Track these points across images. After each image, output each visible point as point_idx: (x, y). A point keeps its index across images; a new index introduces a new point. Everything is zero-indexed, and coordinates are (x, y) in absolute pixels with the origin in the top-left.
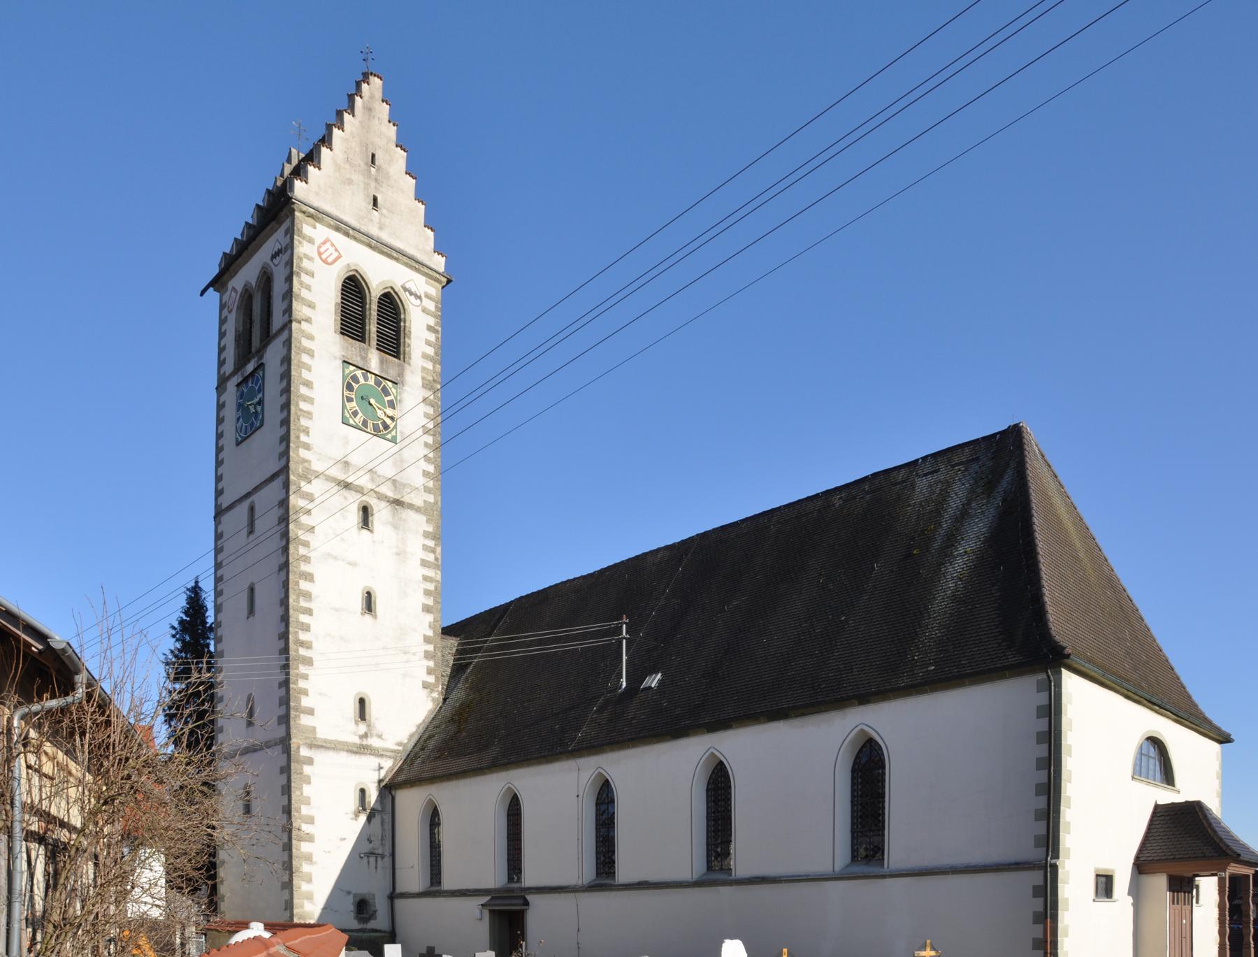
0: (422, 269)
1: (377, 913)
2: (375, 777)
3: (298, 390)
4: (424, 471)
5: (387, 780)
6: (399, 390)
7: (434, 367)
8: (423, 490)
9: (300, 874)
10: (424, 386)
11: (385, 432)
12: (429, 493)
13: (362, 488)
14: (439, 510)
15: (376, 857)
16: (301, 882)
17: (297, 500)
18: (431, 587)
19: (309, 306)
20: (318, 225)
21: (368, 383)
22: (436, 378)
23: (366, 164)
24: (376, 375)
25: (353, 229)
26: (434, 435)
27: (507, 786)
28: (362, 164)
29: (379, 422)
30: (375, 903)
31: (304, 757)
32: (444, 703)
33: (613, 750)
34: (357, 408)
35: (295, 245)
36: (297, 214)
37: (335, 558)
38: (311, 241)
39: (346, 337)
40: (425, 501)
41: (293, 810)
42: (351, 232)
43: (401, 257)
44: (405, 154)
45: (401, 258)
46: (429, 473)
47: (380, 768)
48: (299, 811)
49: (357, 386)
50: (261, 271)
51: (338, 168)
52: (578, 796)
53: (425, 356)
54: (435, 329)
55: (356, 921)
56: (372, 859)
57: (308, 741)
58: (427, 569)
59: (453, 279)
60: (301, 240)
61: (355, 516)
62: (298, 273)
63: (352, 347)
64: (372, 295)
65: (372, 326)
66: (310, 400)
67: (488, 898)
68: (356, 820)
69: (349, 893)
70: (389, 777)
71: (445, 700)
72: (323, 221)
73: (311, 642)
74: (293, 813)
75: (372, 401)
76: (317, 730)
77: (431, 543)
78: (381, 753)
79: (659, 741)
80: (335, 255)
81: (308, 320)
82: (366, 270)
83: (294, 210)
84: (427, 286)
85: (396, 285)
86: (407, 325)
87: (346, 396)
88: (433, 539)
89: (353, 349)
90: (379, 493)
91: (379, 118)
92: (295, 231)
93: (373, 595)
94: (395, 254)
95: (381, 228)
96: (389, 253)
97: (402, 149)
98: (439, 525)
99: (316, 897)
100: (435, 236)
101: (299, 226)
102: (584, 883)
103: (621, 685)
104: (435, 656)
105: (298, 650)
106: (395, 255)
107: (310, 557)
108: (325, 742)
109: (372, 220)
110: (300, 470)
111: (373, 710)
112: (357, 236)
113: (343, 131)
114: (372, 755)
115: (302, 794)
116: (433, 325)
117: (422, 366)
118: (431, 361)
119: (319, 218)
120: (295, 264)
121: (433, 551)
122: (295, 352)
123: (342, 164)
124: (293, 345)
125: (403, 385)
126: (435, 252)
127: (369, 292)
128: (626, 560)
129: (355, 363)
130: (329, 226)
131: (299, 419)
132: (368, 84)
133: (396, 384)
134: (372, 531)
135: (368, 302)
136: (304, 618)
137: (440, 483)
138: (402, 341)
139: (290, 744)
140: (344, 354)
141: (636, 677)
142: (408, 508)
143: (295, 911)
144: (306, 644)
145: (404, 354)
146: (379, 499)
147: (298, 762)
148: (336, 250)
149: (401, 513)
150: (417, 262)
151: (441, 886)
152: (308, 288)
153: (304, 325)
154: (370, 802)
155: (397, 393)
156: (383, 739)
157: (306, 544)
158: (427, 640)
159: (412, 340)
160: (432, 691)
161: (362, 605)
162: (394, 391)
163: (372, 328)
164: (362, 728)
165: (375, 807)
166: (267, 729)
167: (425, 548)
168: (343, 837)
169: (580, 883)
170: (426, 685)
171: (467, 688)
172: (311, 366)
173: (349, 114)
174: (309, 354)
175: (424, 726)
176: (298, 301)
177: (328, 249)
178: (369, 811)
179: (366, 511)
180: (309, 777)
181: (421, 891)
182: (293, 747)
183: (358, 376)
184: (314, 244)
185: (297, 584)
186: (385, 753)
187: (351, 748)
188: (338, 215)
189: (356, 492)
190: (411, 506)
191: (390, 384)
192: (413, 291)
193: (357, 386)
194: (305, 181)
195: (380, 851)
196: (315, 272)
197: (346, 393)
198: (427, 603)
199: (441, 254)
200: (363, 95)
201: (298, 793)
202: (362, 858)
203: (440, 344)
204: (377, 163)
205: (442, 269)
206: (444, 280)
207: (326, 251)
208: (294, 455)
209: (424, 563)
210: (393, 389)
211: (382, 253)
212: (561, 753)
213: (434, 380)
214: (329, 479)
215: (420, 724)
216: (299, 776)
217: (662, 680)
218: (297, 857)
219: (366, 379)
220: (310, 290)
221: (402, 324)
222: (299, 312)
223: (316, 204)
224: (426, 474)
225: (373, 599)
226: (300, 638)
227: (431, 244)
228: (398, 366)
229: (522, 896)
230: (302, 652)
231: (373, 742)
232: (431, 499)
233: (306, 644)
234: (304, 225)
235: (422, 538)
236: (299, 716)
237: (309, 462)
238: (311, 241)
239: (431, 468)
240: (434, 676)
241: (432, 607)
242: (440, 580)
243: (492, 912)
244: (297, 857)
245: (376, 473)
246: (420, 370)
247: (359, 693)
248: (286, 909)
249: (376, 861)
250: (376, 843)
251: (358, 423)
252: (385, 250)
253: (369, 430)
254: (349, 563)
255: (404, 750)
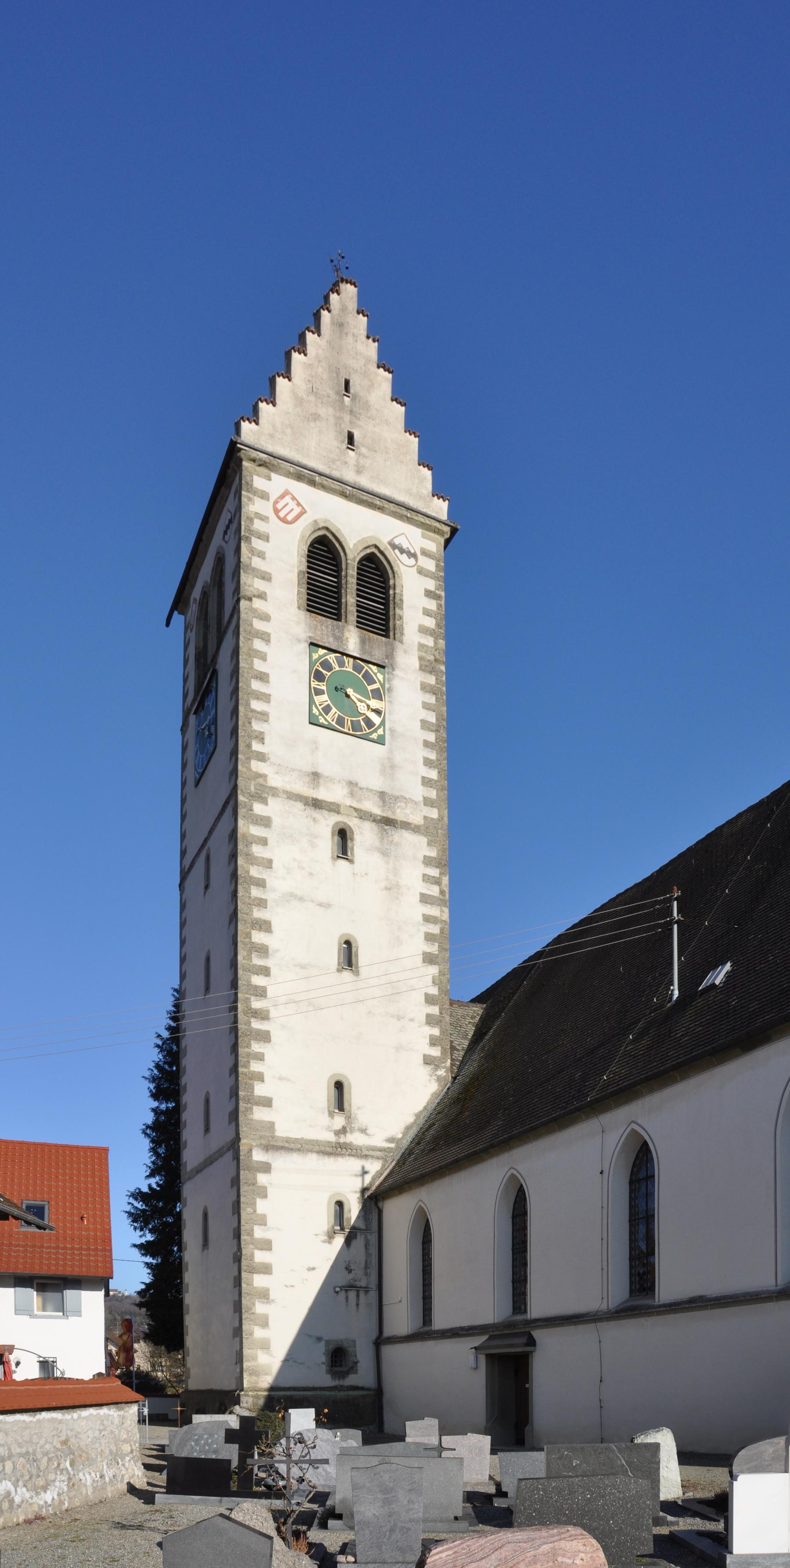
0: (416, 518)
1: (359, 1365)
2: (357, 1184)
3: (249, 686)
4: (423, 778)
5: (374, 1188)
6: (386, 675)
7: (435, 643)
8: (422, 803)
9: (252, 1317)
10: (422, 668)
11: (368, 731)
12: (432, 807)
13: (338, 806)
14: (445, 827)
15: (358, 1291)
16: (253, 1326)
17: (249, 827)
18: (435, 929)
19: (263, 578)
20: (274, 476)
21: (344, 669)
22: (438, 657)
23: (338, 393)
24: (355, 658)
25: (320, 474)
26: (437, 731)
27: (509, 1174)
28: (331, 393)
29: (360, 718)
30: (355, 1351)
31: (257, 1162)
32: (453, 1083)
33: (652, 1091)
34: (329, 702)
35: (243, 503)
36: (245, 464)
37: (301, 899)
38: (264, 496)
39: (313, 615)
40: (425, 818)
41: (242, 1232)
42: (318, 479)
43: (386, 505)
44: (390, 376)
45: (386, 506)
46: (430, 780)
47: (364, 1172)
48: (251, 1233)
49: (329, 674)
50: (216, 557)
51: (299, 401)
52: (602, 1173)
53: (423, 630)
54: (436, 595)
55: (329, 1376)
56: (352, 1295)
57: (263, 1142)
58: (429, 906)
59: (459, 527)
60: (250, 495)
61: (327, 843)
62: (247, 537)
63: (322, 625)
64: (348, 558)
65: (348, 597)
66: (265, 698)
67: (484, 1338)
68: (330, 1243)
69: (319, 1339)
70: (377, 1183)
71: (454, 1078)
72: (280, 468)
73: (268, 1011)
74: (242, 1237)
75: (350, 691)
76: (277, 1127)
77: (434, 872)
78: (365, 1152)
79: (721, 1061)
80: (297, 510)
81: (262, 596)
82: (339, 526)
83: (241, 460)
84: (425, 540)
85: (380, 541)
86: (397, 591)
87: (314, 687)
88: (437, 867)
89: (323, 627)
90: (361, 810)
91: (353, 335)
92: (243, 486)
93: (353, 945)
94: (378, 502)
95: (359, 471)
96: (370, 500)
97: (385, 370)
98: (445, 847)
99: (274, 1346)
100: (433, 475)
101: (248, 479)
102: (610, 1306)
103: (672, 995)
104: (441, 1021)
105: (250, 1022)
106: (378, 503)
107: (266, 901)
108: (287, 1142)
109: (346, 463)
110: (252, 788)
111: (355, 1097)
112: (325, 483)
113: (305, 355)
114: (353, 1156)
115: (255, 1211)
116: (433, 589)
117: (419, 643)
118: (431, 635)
119: (273, 465)
120: (243, 528)
121: (437, 882)
122: (244, 637)
123: (305, 397)
124: (241, 629)
125: (393, 669)
126: (433, 496)
127: (345, 554)
128: (694, 845)
129: (327, 645)
130: (288, 475)
131: (250, 723)
132: (339, 294)
133: (383, 667)
134: (351, 861)
135: (344, 567)
136: (258, 980)
137: (446, 792)
138: (391, 613)
139: (239, 1147)
140: (311, 634)
141: (690, 980)
142: (402, 828)
143: (246, 1365)
144: (261, 1013)
145: (394, 629)
146: (361, 818)
147: (249, 1168)
148: (299, 504)
149: (392, 835)
150: (409, 509)
151: (431, 1325)
152: (262, 555)
153: (257, 603)
154: (350, 1219)
155: (384, 678)
156: (367, 1134)
157: (261, 884)
158: (430, 1000)
159: (404, 611)
160: (437, 1067)
161: (339, 959)
162: (380, 677)
163: (350, 599)
164: (339, 1121)
165: (357, 1225)
166: (220, 1135)
167: (426, 878)
168: (311, 1266)
169: (604, 1307)
170: (428, 1060)
171: (482, 1058)
172: (266, 654)
173: (313, 333)
174: (262, 639)
175: (426, 1114)
176: (248, 574)
177: (287, 504)
178: (347, 1230)
179: (343, 835)
180: (264, 1188)
181: (410, 1332)
182: (243, 1149)
183: (331, 661)
184: (268, 500)
185: (249, 935)
186: (371, 1153)
187: (323, 1148)
188: (300, 460)
189: (330, 811)
190: (406, 826)
191: (374, 668)
192: (405, 547)
193: (329, 674)
194: (255, 421)
195: (363, 1283)
196: (270, 534)
197: (315, 684)
198: (428, 950)
199: (442, 497)
200: (332, 307)
201: (249, 1210)
202: (337, 1292)
203: (444, 613)
204: (352, 390)
205: (444, 516)
206: (447, 529)
207: (284, 506)
208: (245, 770)
209: (425, 899)
210: (378, 675)
211: (361, 502)
212: (578, 1109)
213: (436, 660)
214: (293, 796)
215: (421, 1112)
216: (251, 1187)
217: (731, 971)
218: (248, 1294)
219: (341, 664)
220: (264, 558)
221: (391, 592)
222: (249, 586)
223: (270, 448)
224: (426, 782)
225: (354, 950)
226: (253, 1007)
227: (428, 486)
228: (386, 645)
229: (527, 1332)
230: (256, 1025)
231: (355, 1139)
232: (434, 814)
233: (261, 1013)
234: (255, 478)
235: (422, 866)
236: (251, 1109)
237: (264, 776)
238: (264, 496)
239: (433, 774)
240: (439, 1048)
241: (437, 956)
242: (448, 920)
243: (489, 1357)
244: (248, 1294)
245: (357, 784)
246: (416, 648)
247: (334, 1075)
248: (236, 1363)
249: (358, 1296)
250: (358, 1272)
251: (330, 721)
252: (364, 498)
253: (346, 730)
254: (320, 905)
255: (397, 1147)
